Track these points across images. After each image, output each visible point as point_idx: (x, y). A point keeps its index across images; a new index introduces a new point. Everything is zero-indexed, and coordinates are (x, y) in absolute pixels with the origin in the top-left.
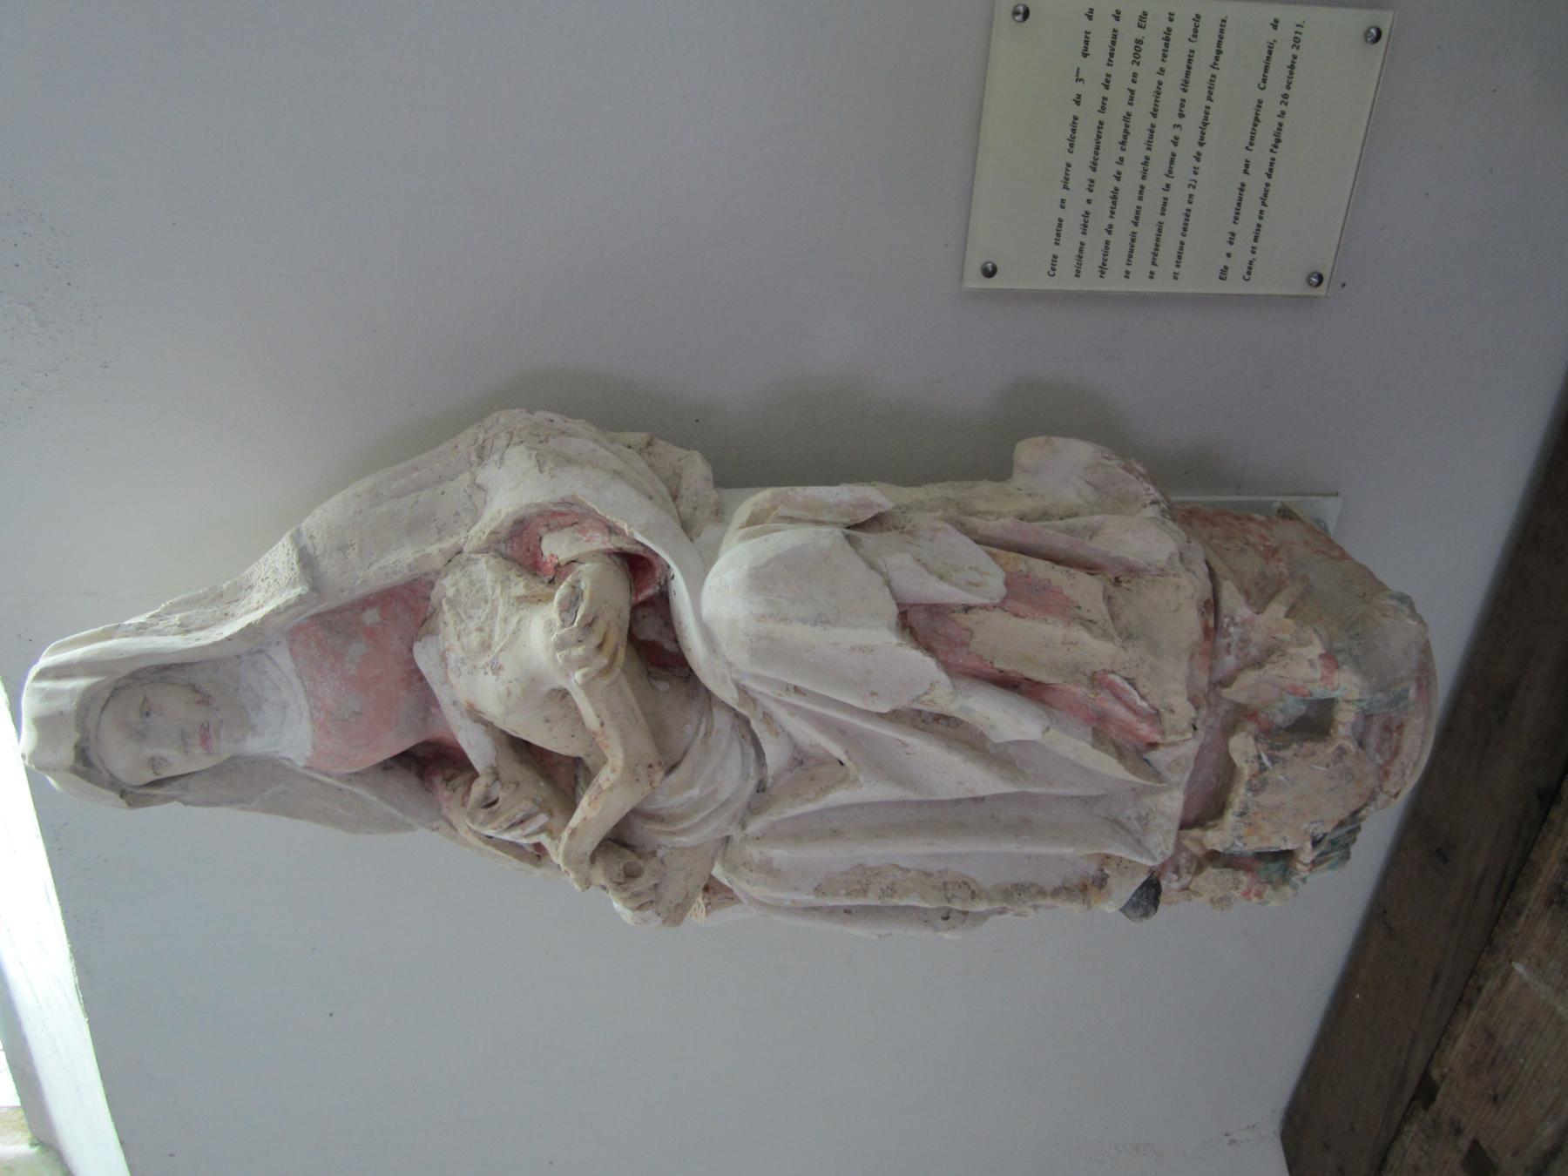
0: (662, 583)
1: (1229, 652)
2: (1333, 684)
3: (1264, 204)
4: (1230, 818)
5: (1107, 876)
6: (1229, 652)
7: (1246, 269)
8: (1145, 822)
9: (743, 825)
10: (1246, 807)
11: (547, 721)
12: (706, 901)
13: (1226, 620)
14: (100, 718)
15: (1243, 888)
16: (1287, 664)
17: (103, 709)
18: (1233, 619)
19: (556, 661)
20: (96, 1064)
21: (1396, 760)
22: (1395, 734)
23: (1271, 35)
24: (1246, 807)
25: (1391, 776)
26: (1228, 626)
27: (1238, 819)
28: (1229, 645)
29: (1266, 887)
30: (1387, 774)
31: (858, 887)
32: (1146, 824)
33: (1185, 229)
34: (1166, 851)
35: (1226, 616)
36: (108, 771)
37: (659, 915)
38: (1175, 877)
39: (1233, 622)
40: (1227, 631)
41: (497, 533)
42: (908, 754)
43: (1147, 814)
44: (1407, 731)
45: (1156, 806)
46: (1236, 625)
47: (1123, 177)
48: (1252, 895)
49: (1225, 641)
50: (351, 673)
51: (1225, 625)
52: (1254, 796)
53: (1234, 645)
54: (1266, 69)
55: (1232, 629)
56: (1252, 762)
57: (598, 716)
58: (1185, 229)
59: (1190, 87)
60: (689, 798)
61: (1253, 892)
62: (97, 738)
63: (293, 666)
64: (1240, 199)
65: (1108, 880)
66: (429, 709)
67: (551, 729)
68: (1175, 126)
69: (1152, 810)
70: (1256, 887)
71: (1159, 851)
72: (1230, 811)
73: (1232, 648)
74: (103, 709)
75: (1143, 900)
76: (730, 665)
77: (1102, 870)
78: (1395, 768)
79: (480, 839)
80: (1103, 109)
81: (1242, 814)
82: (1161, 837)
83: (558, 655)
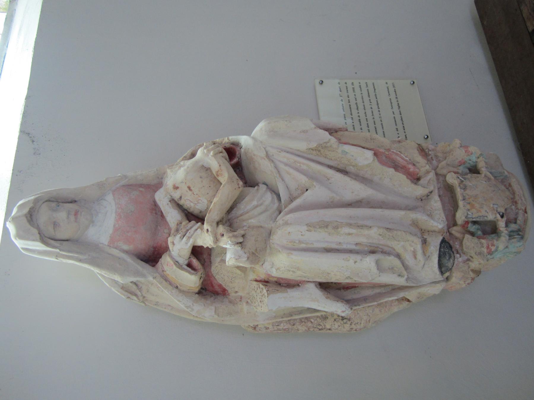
0: (239, 157)
1: (433, 160)
2: (470, 151)
3: (402, 121)
4: (461, 203)
5: (426, 238)
6: (433, 160)
7: (405, 137)
8: (431, 215)
9: (275, 220)
10: (464, 197)
11: (201, 177)
12: (267, 289)
13: (427, 150)
14: (41, 205)
15: (485, 245)
16: (452, 154)
17: (44, 203)
18: (429, 149)
19: (205, 152)
20: (39, 21)
21: (516, 195)
22: (510, 188)
23: (387, 85)
24: (464, 197)
25: (518, 202)
26: (428, 152)
27: (464, 201)
28: (432, 158)
29: (494, 241)
30: (516, 203)
31: (323, 226)
32: (431, 216)
33: (383, 128)
34: (443, 219)
35: (426, 149)
36: (37, 224)
37: (245, 253)
38: (458, 255)
39: (429, 150)
40: (429, 154)
41: (186, 157)
42: (330, 183)
43: (430, 213)
44: (512, 184)
45: (432, 208)
46: (430, 151)
47: (363, 129)
48: (490, 247)
49: (430, 157)
50: (133, 197)
51: (427, 152)
52: (465, 191)
53: (433, 157)
54: (389, 92)
55: (430, 153)
56: (457, 179)
57: (219, 163)
58: (383, 128)
59: (370, 96)
60: (253, 205)
61: (490, 245)
62: (38, 211)
63: (113, 198)
64: (395, 120)
65: (427, 240)
66: (157, 226)
67: (202, 182)
68: (370, 105)
69: (431, 211)
70: (490, 243)
71: (440, 221)
72: (459, 201)
73: (433, 158)
74: (44, 203)
75: (445, 249)
76: (261, 142)
77: (423, 237)
78: (517, 198)
79: (173, 261)
80: (349, 102)
81: (464, 200)
82: (439, 216)
83: (205, 150)
